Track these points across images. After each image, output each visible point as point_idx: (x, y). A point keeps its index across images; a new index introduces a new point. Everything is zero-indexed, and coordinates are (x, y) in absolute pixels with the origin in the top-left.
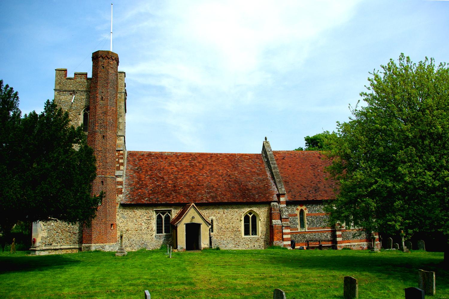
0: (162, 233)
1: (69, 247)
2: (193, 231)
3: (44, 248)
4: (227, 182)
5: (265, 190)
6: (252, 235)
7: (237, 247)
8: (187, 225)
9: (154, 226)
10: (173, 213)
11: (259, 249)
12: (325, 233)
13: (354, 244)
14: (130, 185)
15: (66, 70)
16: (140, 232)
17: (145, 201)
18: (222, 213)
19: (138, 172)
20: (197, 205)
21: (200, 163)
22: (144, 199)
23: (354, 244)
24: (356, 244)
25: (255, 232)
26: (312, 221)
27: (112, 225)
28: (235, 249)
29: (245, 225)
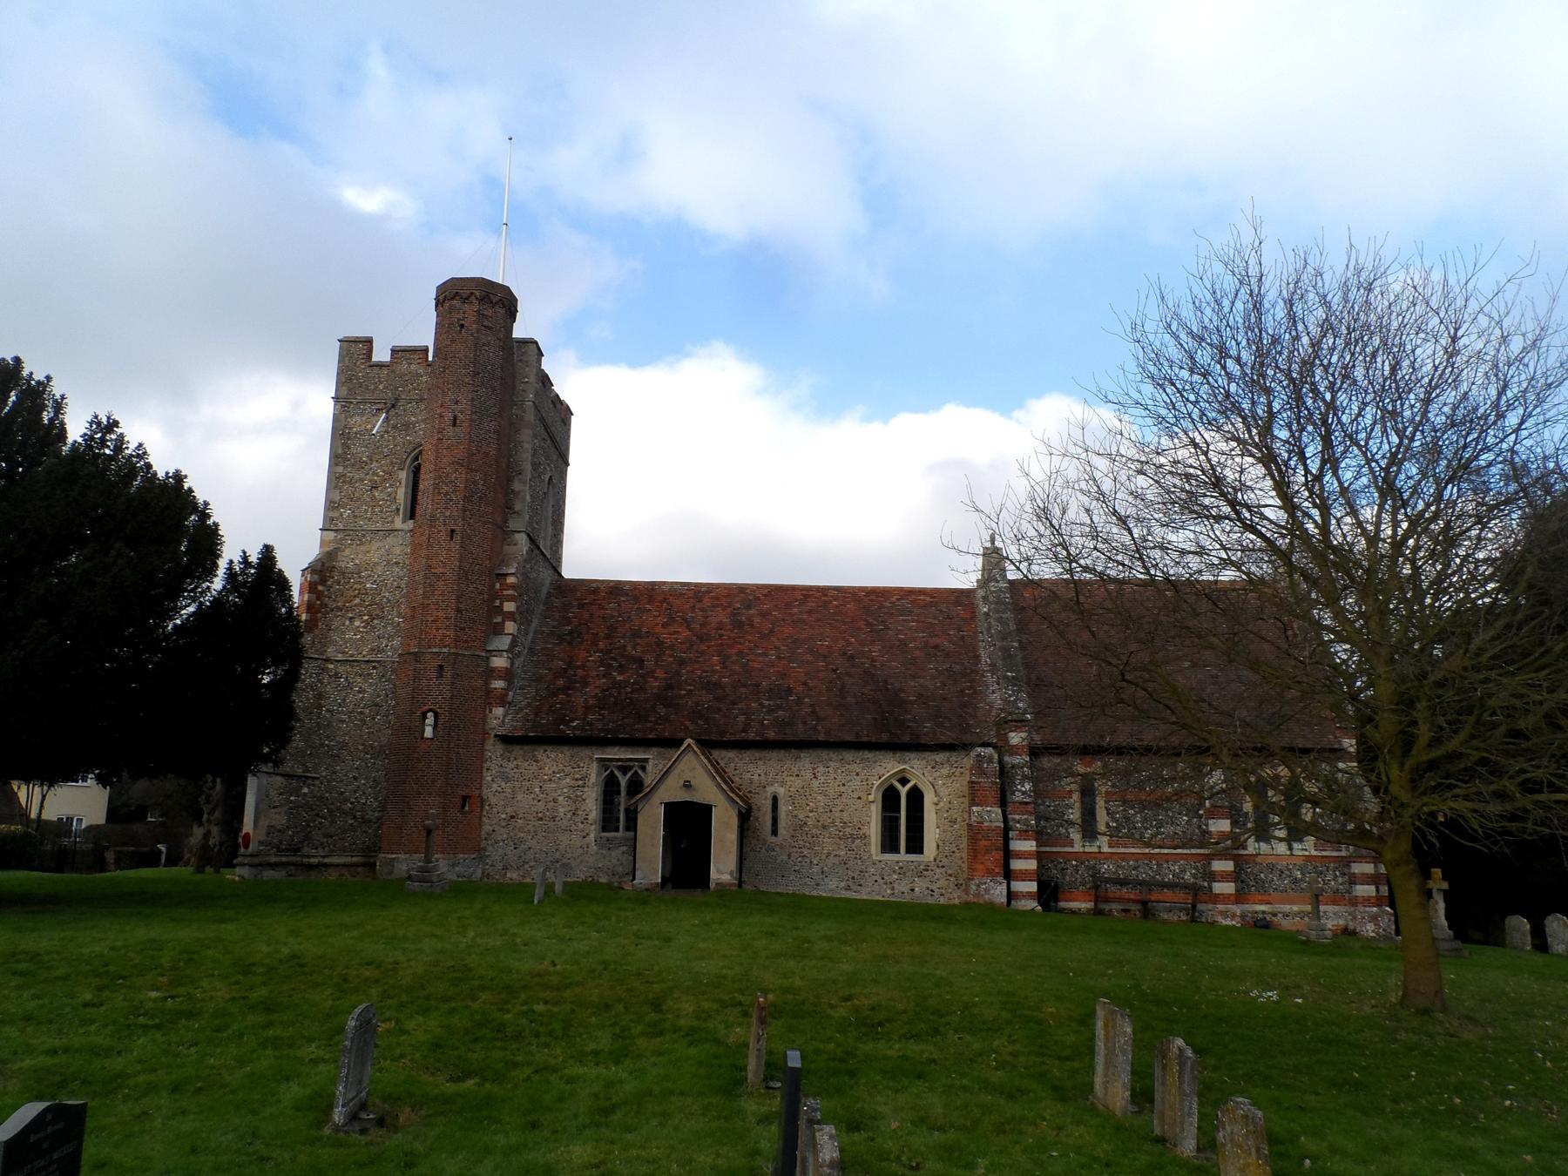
0: (617, 830)
1: (348, 860)
2: (688, 825)
3: (274, 859)
4: (838, 678)
5: (964, 705)
6: (908, 851)
7: (854, 888)
8: (670, 808)
9: (592, 805)
10: (649, 767)
11: (930, 901)
12: (1175, 862)
13: (1287, 908)
14: (538, 679)
15: (368, 342)
16: (551, 824)
17: (573, 727)
18: (809, 775)
19: (570, 643)
20: (700, 742)
21: (764, 614)
22: (567, 723)
23: (1287, 908)
24: (1295, 908)
25: (916, 845)
26: (1127, 819)
27: (465, 799)
28: (848, 895)
29: (884, 819)
